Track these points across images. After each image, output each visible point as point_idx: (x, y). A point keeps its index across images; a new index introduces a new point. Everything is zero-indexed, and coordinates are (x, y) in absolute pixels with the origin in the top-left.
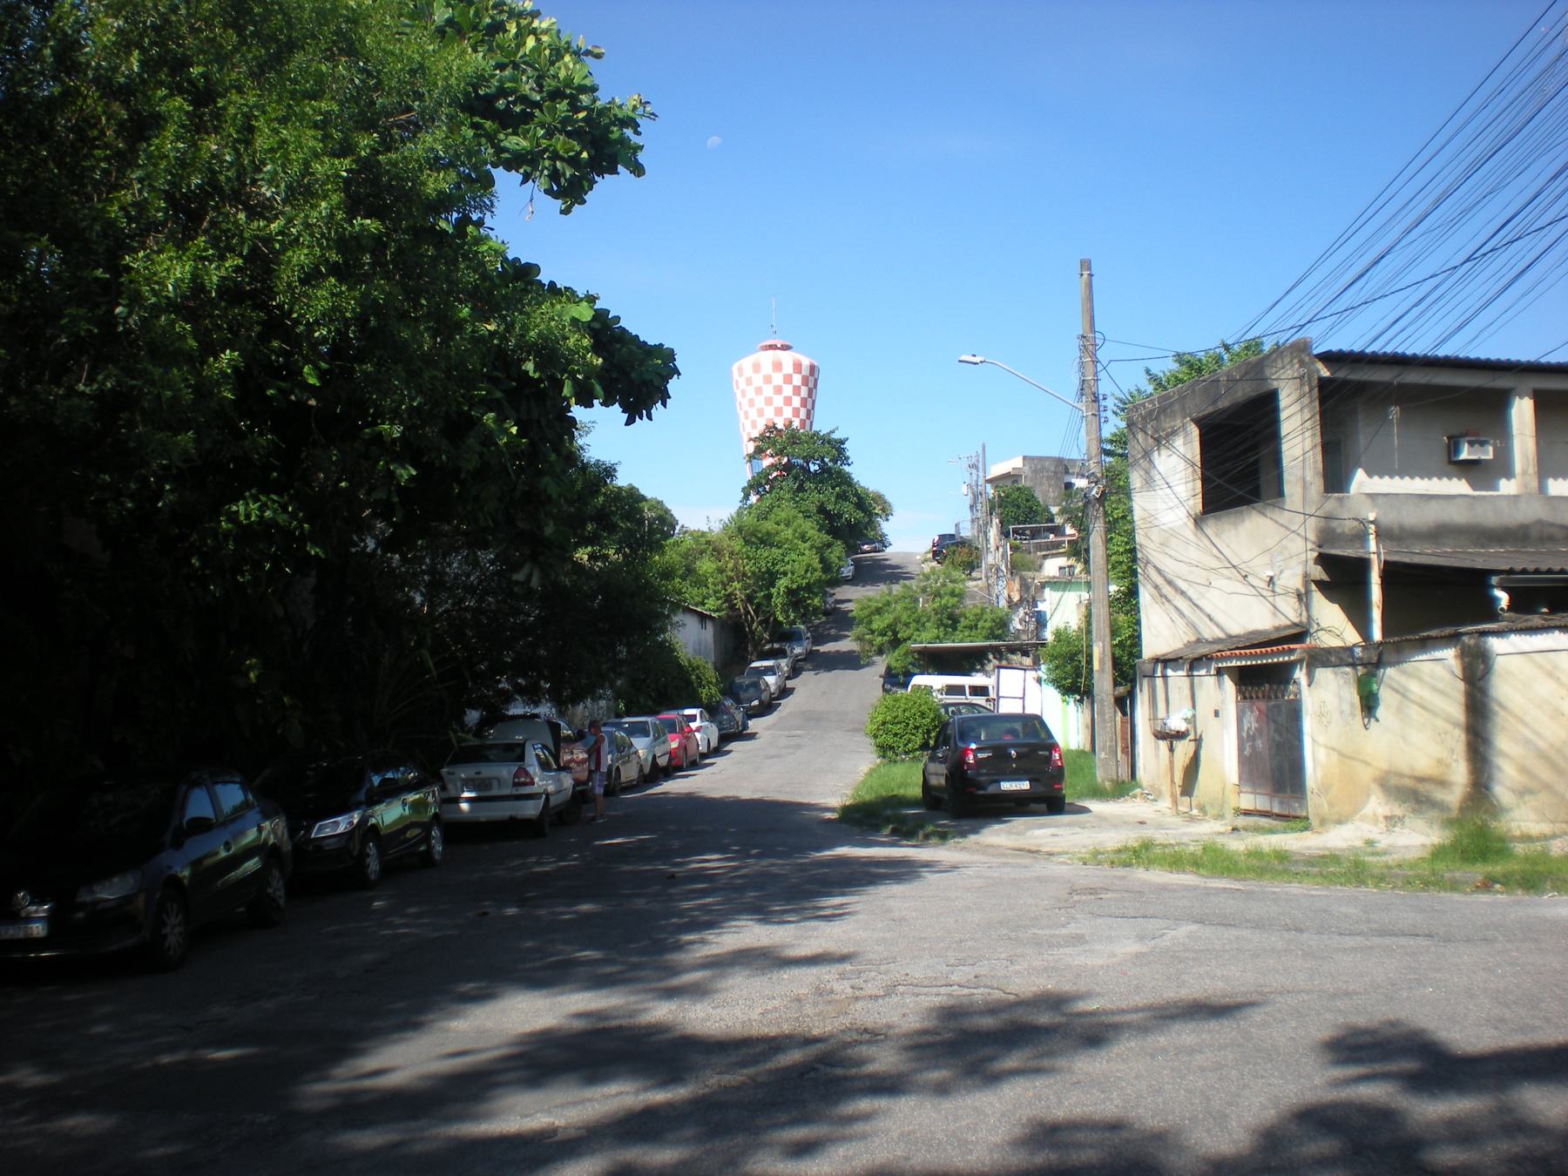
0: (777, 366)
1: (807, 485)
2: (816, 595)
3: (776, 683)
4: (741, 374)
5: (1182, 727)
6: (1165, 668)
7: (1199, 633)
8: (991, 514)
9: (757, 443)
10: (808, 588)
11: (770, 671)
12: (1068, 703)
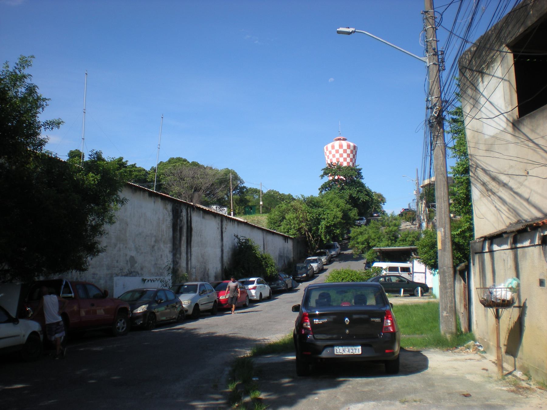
2: (338, 228)
5: (508, 296)
6: (491, 244)
7: (519, 215)
10: (335, 225)
11: (314, 261)
12: (434, 275)
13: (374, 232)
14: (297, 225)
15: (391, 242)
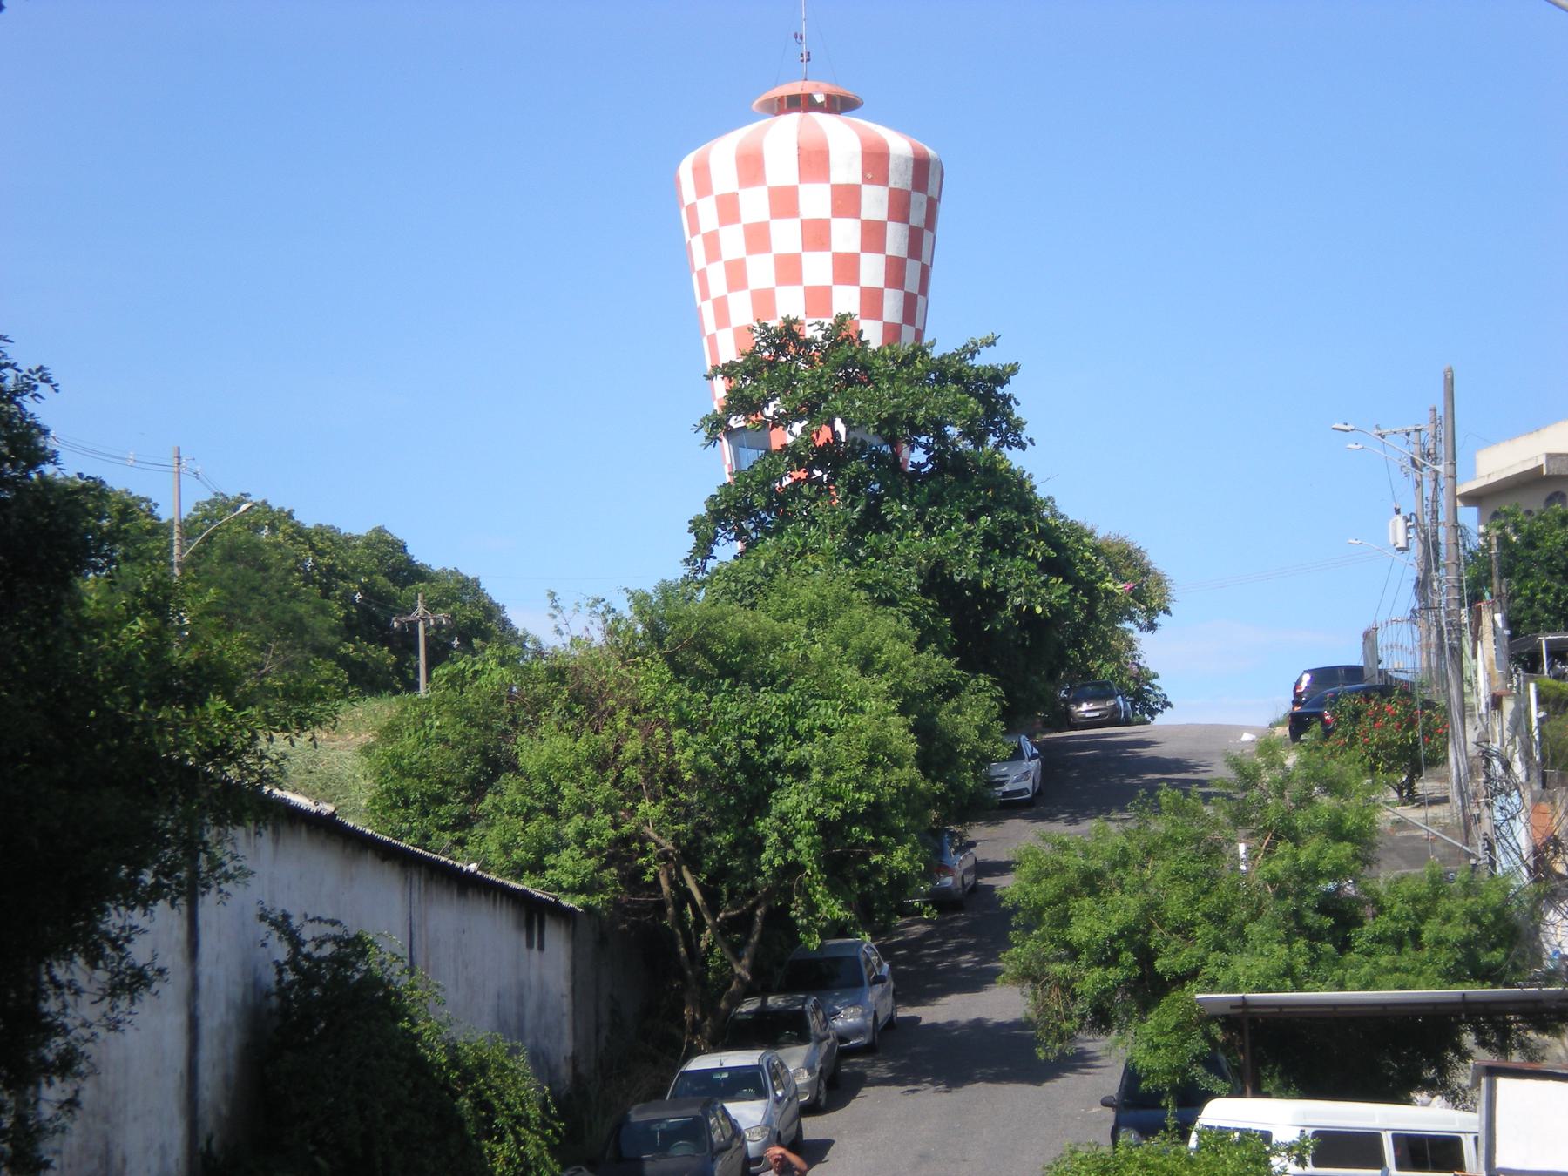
0: (814, 161)
1: (894, 509)
3: (768, 1124)
4: (703, 188)
8: (1476, 598)
9: (737, 382)
10: (875, 815)
11: (746, 1083)
13: (1179, 876)
14: (601, 820)
15: (1312, 948)
